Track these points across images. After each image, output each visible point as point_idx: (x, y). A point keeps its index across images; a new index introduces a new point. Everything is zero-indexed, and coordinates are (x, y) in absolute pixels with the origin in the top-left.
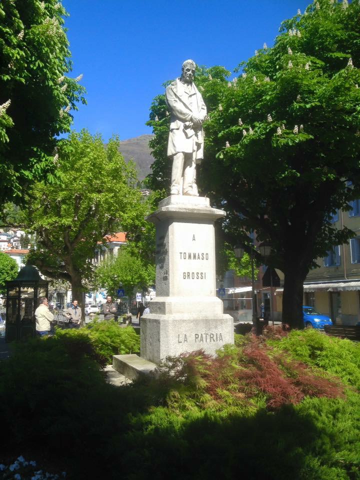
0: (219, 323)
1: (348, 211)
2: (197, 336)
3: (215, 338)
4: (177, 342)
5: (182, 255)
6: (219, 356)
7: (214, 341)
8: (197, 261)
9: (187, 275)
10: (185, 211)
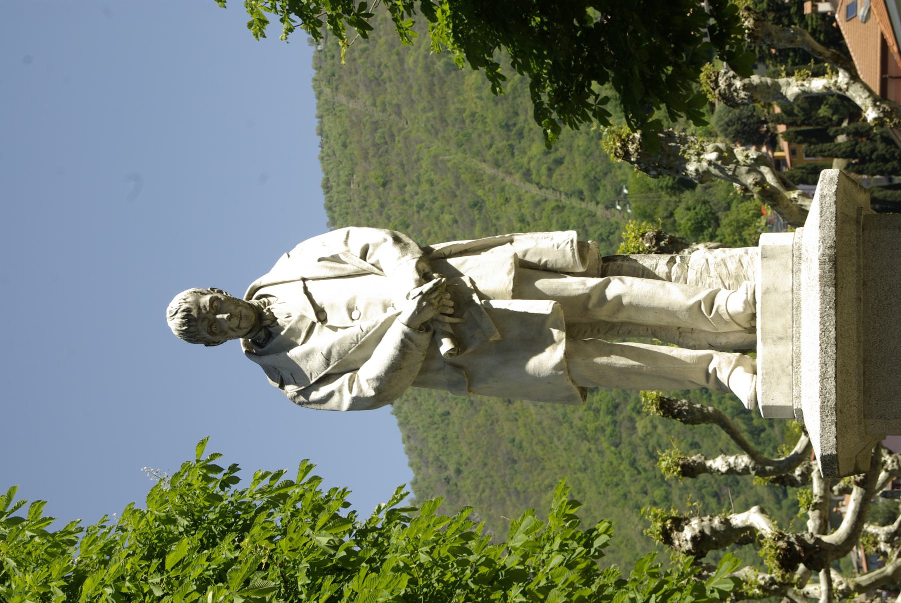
10: (831, 384)
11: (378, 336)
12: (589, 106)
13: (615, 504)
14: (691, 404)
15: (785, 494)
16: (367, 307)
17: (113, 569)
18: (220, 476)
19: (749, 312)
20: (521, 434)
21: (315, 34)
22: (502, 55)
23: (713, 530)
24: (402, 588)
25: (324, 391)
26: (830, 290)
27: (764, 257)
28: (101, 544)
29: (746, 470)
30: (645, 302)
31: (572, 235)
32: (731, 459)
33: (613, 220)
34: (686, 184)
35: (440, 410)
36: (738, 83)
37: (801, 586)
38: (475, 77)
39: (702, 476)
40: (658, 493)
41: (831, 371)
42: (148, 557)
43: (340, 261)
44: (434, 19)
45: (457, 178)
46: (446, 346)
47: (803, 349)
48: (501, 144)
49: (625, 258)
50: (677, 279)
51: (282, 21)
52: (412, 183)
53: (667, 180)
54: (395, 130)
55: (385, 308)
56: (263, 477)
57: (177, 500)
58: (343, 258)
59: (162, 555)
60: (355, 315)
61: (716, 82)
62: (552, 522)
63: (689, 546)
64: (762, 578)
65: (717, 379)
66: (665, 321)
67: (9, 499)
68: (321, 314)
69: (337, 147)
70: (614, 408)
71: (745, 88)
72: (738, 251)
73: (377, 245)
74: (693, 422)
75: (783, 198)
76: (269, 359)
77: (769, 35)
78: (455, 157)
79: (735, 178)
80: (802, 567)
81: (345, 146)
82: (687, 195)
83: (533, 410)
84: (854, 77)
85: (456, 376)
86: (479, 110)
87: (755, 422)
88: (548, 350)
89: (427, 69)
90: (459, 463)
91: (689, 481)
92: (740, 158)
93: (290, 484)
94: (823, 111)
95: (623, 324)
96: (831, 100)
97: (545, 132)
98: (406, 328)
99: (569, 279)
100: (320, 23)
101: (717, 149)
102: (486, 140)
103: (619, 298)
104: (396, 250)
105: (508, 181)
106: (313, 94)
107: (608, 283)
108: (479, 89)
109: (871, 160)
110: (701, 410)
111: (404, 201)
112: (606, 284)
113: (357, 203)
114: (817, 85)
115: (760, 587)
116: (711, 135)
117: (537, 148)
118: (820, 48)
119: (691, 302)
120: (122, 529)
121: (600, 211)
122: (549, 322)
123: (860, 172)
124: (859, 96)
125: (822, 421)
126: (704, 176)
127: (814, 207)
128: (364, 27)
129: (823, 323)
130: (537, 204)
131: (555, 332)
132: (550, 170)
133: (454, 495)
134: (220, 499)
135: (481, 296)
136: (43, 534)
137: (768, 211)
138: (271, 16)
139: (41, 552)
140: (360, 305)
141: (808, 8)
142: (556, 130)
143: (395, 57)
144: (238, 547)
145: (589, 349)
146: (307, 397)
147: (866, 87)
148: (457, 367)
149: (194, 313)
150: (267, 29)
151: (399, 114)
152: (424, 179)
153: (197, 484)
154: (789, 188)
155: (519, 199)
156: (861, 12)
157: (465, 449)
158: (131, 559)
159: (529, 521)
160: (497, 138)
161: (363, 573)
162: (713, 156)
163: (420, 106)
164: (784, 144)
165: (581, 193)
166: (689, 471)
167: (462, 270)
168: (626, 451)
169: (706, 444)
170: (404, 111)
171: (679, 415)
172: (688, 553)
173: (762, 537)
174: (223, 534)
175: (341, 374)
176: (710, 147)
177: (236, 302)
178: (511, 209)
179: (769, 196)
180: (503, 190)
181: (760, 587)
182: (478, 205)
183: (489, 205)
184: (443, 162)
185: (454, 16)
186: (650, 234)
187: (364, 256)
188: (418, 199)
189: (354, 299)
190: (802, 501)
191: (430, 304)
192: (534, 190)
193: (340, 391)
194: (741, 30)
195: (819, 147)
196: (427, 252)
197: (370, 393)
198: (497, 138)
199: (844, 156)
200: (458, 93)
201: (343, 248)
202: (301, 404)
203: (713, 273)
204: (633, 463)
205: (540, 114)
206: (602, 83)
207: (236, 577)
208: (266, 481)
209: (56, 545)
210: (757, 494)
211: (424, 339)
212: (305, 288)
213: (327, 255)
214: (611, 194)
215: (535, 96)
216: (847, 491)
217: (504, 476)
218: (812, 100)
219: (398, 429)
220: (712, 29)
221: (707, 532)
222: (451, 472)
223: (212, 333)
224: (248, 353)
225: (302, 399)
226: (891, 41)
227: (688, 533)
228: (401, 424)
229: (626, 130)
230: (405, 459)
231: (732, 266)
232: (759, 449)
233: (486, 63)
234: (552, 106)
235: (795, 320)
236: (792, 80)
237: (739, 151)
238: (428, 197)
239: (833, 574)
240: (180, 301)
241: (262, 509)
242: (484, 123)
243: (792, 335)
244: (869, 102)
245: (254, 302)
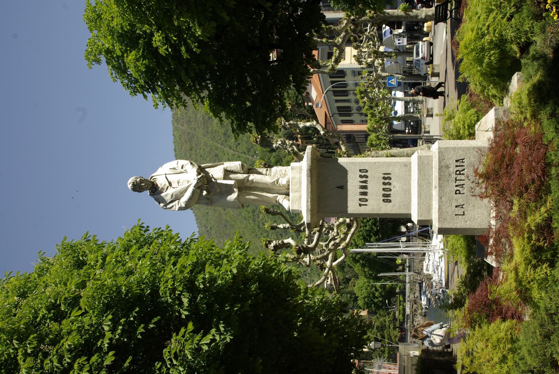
0: (443, 164)
1: (491, 149)
4: (464, 217)
8: (369, 185)
9: (387, 198)
10: (309, 204)
11: (186, 190)
12: (247, 128)
13: (253, 237)
14: (274, 210)
15: (299, 234)
16: (183, 182)
17: (115, 254)
18: (144, 229)
19: (288, 184)
20: (228, 219)
21: (171, 108)
22: (223, 114)
23: (279, 244)
24: (195, 260)
25: (171, 205)
26: (309, 178)
27: (292, 169)
28: (112, 247)
29: (288, 228)
30: (260, 181)
31: (240, 162)
32: (284, 225)
33: (254, 160)
34: (273, 150)
35: (206, 212)
36: (287, 123)
37: (302, 259)
38: (216, 121)
39: (277, 230)
40: (265, 235)
41: (309, 200)
42: (125, 251)
43: (176, 169)
44: (204, 104)
45: (211, 148)
46: (205, 193)
47: (302, 194)
48: (223, 139)
49: (255, 169)
50: (269, 175)
51: (163, 104)
52: (199, 149)
53: (269, 149)
54: (194, 135)
55: (188, 182)
56: (156, 229)
57: (132, 236)
58: (176, 168)
59: (128, 250)
60: (179, 184)
61: (281, 123)
62: (235, 242)
63: (273, 248)
64: (292, 257)
65: (279, 203)
66: (265, 186)
67: (87, 235)
68: (170, 184)
69: (178, 139)
70: (254, 211)
71: (289, 124)
72: (285, 167)
73: (186, 165)
74: (274, 215)
75: (299, 154)
76: (155, 196)
77: (295, 110)
78: (211, 142)
79: (286, 149)
80: (303, 254)
81: (180, 139)
82: (274, 153)
83: (231, 212)
84: (318, 122)
85: (207, 201)
86: (217, 130)
87: (292, 215)
88: (233, 194)
89: (203, 118)
90: (211, 227)
91: (274, 231)
92: (287, 143)
93: (163, 231)
94: (310, 132)
95: (253, 187)
96: (312, 129)
97: (235, 136)
98: (194, 188)
99: (239, 175)
100: (173, 105)
101: (281, 141)
102: (219, 138)
103: (252, 180)
104: (191, 166)
105: (225, 149)
106: (172, 125)
107: (249, 176)
108: (217, 124)
109: (323, 145)
110: (276, 212)
111: (196, 154)
112: (249, 176)
113: (183, 154)
114: (308, 124)
115: (291, 259)
116: (280, 137)
117: (233, 140)
118: (309, 114)
119: (272, 181)
120: (117, 243)
121: (250, 157)
122: (234, 186)
123: (320, 148)
124: (319, 128)
125: (307, 213)
126: (278, 148)
127: (305, 156)
128: (185, 106)
129: (307, 187)
130: (233, 155)
131: (235, 189)
132: (236, 146)
133: (210, 235)
134: (144, 235)
135: (215, 179)
136: (96, 244)
137: (295, 158)
138: (159, 103)
139: (95, 249)
140: (181, 181)
141: (306, 104)
142: (238, 135)
143: (194, 115)
144: (149, 248)
145: (244, 194)
146: (166, 207)
147: (321, 125)
148: (208, 199)
149: (135, 183)
150: (158, 106)
151: (195, 130)
152: (202, 148)
153: (138, 231)
154: (300, 151)
155: (228, 154)
156: (320, 105)
157: (213, 222)
158: (120, 252)
159: (230, 241)
160: (222, 137)
161: (183, 256)
162: (280, 143)
163: (201, 129)
164: (300, 140)
165: (245, 152)
166: (273, 228)
167: (209, 172)
168: (257, 223)
169: (278, 221)
170: (197, 130)
171: (270, 213)
172: (272, 250)
173: (292, 246)
174: (145, 245)
175: (176, 200)
176: (279, 140)
177: (147, 180)
178: (226, 156)
179: (295, 154)
180: (223, 151)
181: (291, 259)
182: (216, 155)
183: (220, 155)
184: (207, 144)
185: (210, 104)
186: (263, 163)
187: (182, 168)
188: (200, 154)
189: (179, 180)
190: (303, 236)
191: (200, 181)
192: (232, 152)
193: (175, 205)
194: (287, 109)
195: (309, 141)
196: (200, 167)
197: (184, 206)
198: (222, 137)
199: (316, 143)
200: (212, 125)
201: (177, 166)
202: (165, 209)
203: (278, 173)
204: (259, 226)
205: (233, 131)
206: (250, 122)
207: (148, 256)
208: (157, 231)
209: (99, 247)
210: (292, 235)
211: (198, 191)
212: (166, 177)
213: (172, 168)
214: (253, 153)
215: (232, 126)
216: (315, 233)
217: (223, 230)
218: (307, 128)
219: (194, 217)
220: (280, 108)
221: (278, 244)
222: (209, 229)
223: (140, 189)
224: (150, 194)
225: (165, 207)
226: (327, 113)
227: (272, 245)
228: (195, 216)
229: (257, 135)
230: (196, 225)
231: (283, 172)
232: (293, 222)
233: (219, 117)
234: (237, 129)
235: (300, 186)
236: (301, 123)
237: (287, 142)
238: (203, 153)
239: (311, 255)
240: (131, 180)
241: (155, 238)
242: (219, 133)
243: (299, 191)
244: (321, 129)
245: (152, 180)
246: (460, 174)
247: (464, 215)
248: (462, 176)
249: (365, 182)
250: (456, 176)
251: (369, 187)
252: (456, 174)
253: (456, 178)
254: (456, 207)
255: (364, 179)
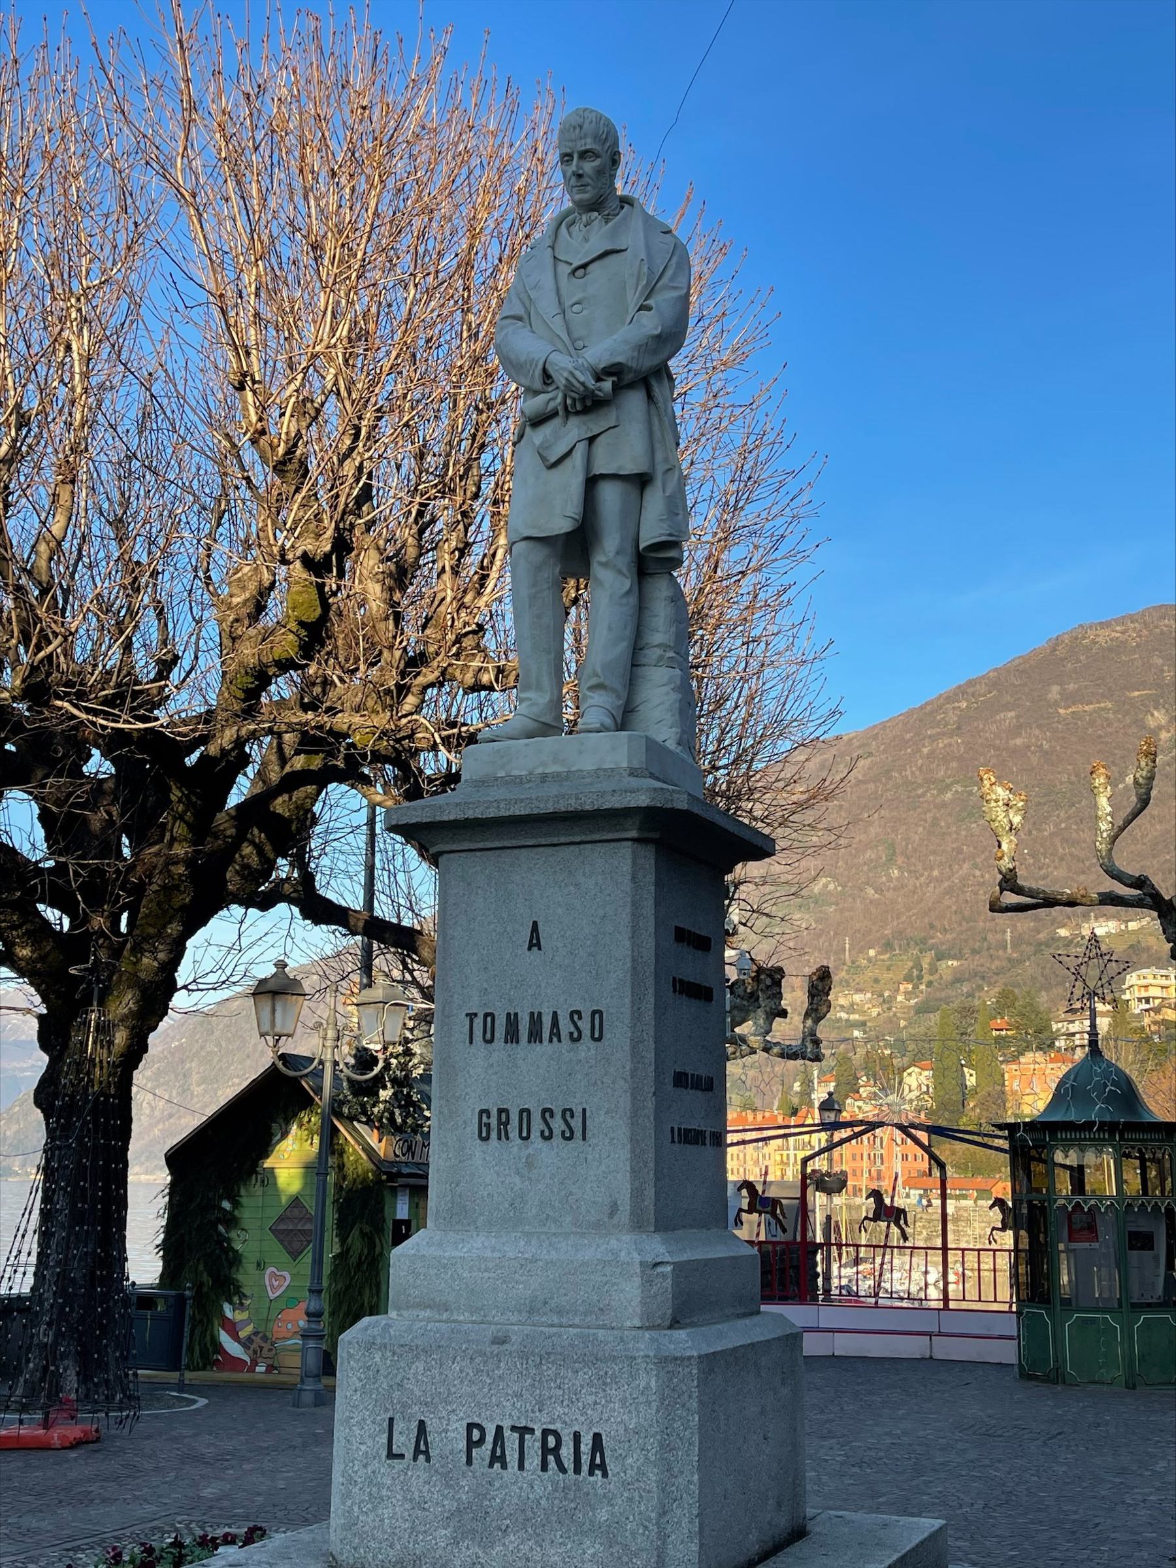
2: (476, 1434)
3: (567, 1452)
5: (478, 1022)
6: (999, 1203)
7: (562, 1469)
8: (545, 1048)
246: (545, 1451)
247: (391, 1455)
248: (537, 1461)
249: (555, 1032)
250: (538, 1433)
251: (537, 1047)
252: (546, 1432)
253: (532, 1431)
254: (422, 1424)
255: (565, 1026)
